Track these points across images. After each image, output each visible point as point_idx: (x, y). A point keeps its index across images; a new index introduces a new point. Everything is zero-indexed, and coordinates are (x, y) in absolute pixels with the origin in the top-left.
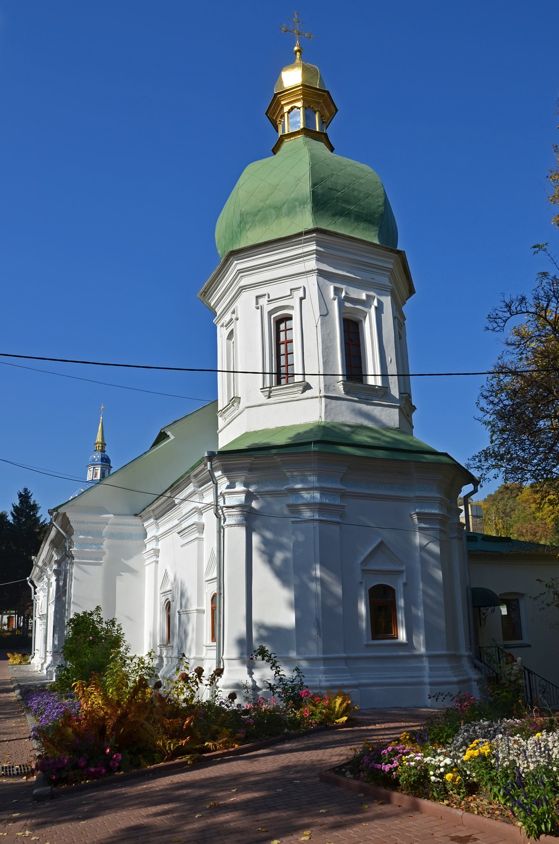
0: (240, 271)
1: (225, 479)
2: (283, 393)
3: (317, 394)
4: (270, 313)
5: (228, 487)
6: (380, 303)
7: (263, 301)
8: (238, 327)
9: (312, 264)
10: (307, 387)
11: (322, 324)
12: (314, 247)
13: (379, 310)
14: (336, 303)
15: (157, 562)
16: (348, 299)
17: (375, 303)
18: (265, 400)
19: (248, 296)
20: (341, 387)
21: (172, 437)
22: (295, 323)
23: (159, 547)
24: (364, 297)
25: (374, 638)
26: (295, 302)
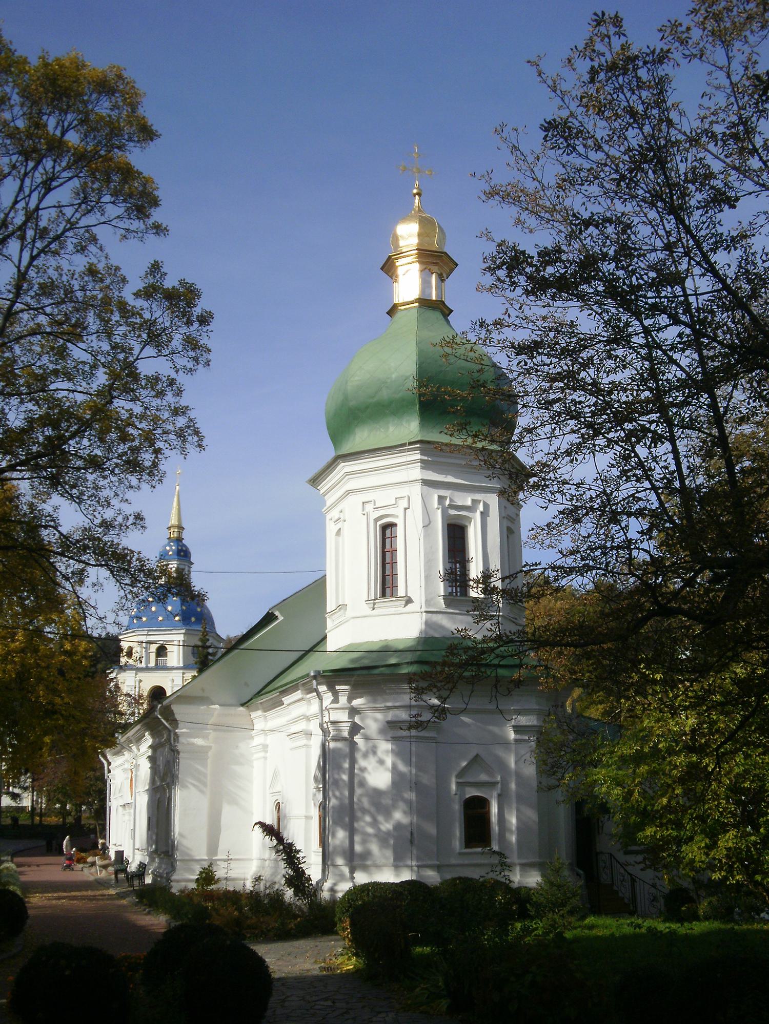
0: (348, 474)
1: (330, 694)
2: (388, 607)
3: (419, 610)
4: (376, 520)
5: (333, 702)
6: (486, 506)
7: (369, 508)
8: (346, 528)
9: (416, 473)
10: (409, 601)
11: (425, 537)
12: (418, 457)
13: (484, 515)
14: (440, 511)
15: (265, 758)
16: (452, 506)
17: (481, 507)
18: (368, 611)
19: (355, 501)
20: (442, 601)
21: (281, 618)
22: (400, 531)
23: (268, 742)
24: (469, 503)
25: (467, 846)
26: (399, 512)
